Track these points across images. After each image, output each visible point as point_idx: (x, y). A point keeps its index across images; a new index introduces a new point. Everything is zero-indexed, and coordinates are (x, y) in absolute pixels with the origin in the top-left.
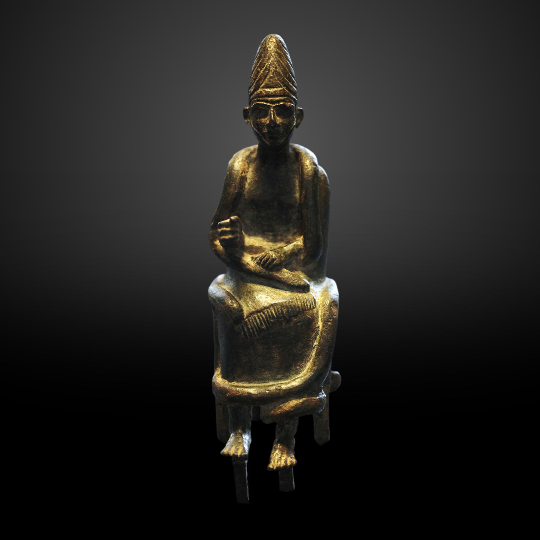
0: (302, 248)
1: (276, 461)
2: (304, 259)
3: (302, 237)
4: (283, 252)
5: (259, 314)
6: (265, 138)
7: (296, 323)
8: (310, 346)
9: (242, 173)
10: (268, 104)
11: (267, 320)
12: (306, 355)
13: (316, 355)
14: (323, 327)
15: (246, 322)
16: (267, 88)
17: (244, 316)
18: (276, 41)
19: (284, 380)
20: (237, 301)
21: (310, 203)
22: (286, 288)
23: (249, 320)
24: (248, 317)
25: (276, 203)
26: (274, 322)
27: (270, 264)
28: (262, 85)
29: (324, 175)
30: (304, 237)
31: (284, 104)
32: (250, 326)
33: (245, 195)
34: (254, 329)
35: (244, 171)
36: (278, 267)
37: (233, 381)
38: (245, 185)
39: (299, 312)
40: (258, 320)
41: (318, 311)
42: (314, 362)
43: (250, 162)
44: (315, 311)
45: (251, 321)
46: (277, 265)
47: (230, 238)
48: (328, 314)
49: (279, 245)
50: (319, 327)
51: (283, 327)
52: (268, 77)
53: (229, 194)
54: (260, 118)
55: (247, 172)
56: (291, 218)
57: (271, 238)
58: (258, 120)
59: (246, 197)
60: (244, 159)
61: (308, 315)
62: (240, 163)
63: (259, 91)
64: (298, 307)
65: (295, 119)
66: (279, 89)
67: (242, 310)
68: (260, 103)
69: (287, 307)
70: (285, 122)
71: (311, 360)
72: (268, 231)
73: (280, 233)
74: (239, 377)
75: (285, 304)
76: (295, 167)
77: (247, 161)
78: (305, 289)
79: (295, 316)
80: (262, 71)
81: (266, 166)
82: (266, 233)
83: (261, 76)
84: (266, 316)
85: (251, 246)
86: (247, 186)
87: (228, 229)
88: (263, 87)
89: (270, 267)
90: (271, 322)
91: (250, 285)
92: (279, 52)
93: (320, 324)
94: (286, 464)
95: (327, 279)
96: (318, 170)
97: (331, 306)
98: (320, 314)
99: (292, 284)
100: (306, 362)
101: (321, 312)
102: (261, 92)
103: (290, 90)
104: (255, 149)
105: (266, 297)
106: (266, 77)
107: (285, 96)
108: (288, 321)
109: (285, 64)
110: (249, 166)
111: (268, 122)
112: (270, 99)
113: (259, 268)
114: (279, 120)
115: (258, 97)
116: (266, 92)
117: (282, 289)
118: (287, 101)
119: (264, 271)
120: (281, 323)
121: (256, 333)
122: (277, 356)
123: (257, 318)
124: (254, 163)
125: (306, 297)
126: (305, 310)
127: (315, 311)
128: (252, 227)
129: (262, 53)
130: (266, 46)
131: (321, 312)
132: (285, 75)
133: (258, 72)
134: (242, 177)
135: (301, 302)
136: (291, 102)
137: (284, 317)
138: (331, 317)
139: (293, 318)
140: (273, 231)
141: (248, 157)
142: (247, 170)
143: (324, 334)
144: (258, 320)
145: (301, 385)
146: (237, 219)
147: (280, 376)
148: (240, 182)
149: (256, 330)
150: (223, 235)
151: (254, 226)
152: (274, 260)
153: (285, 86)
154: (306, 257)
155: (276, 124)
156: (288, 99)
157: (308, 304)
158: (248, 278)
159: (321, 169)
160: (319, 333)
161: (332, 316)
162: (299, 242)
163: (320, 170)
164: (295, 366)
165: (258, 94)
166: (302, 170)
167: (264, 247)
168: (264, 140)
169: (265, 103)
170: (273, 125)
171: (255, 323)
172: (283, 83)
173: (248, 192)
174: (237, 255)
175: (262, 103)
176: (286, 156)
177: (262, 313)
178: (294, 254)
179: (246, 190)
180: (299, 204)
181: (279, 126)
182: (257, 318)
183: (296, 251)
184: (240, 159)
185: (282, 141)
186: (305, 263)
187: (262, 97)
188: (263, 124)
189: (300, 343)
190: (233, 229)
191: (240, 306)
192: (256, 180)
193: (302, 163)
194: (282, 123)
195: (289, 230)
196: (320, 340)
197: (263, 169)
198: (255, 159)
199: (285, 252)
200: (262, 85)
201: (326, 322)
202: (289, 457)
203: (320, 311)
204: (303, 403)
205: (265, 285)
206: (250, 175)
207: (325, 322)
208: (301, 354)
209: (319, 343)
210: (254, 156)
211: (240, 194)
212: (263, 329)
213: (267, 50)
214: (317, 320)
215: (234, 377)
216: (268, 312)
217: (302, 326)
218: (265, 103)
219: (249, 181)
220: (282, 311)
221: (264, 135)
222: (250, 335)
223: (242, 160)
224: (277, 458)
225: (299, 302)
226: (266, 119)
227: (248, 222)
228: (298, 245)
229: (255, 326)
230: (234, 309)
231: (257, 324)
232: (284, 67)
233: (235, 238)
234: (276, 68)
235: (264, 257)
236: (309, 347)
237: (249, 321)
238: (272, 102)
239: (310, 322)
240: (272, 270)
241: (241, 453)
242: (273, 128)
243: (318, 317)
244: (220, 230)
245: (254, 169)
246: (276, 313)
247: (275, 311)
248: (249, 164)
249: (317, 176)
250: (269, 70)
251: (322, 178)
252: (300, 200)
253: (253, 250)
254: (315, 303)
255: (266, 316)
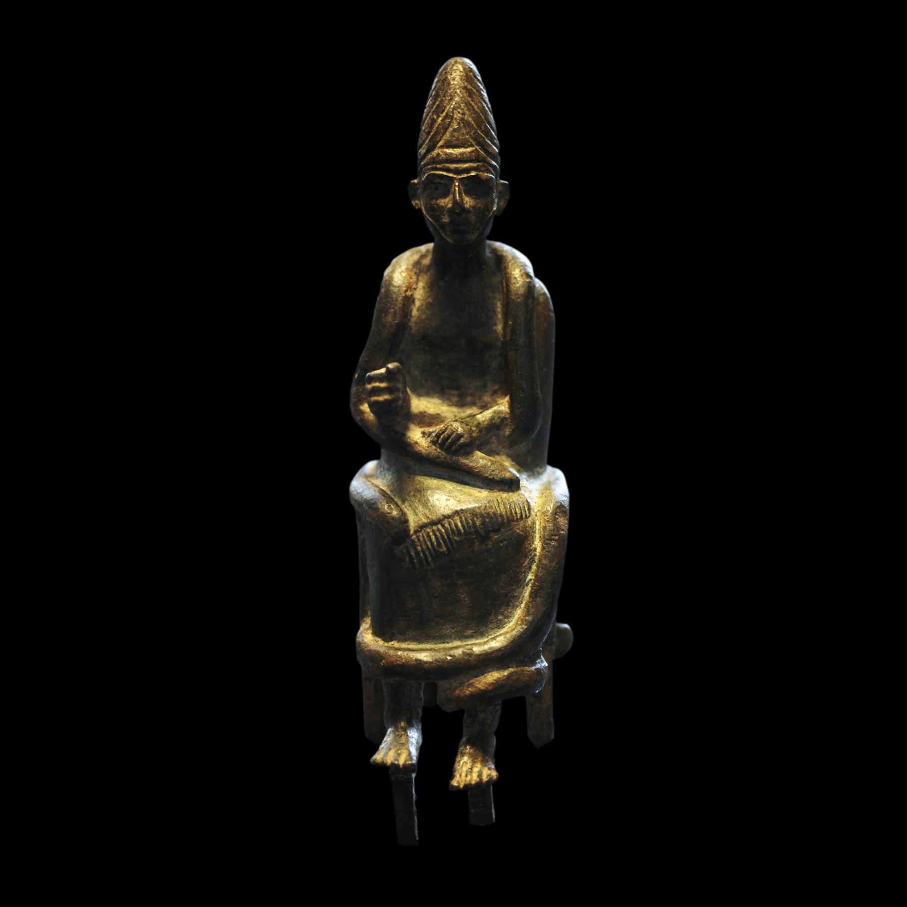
0: (508, 416)
1: (464, 774)
2: (510, 436)
3: (507, 398)
4: (476, 422)
5: (435, 528)
6: (445, 231)
7: (497, 542)
8: (520, 580)
9: (406, 291)
10: (451, 175)
11: (449, 538)
12: (514, 597)
13: (530, 596)
14: (543, 548)
15: (413, 542)
16: (448, 147)
17: (409, 531)
18: (464, 69)
19: (477, 639)
20: (398, 506)
21: (522, 340)
22: (480, 484)
23: (418, 537)
24: (416, 532)
25: (464, 340)
26: (461, 541)
27: (453, 443)
28: (441, 143)
29: (544, 294)
30: (511, 399)
31: (477, 175)
32: (419, 548)
33: (411, 328)
34: (427, 553)
35: (409, 287)
36: (467, 448)
37: (391, 640)
38: (411, 310)
39: (502, 524)
40: (433, 537)
41: (534, 523)
42: (527, 607)
43: (421, 271)
44: (530, 523)
45: (421, 539)
46: (464, 445)
47: (386, 400)
48: (552, 528)
49: (469, 411)
50: (535, 550)
51: (476, 549)
52: (450, 129)
53: (384, 326)
54: (437, 199)
55: (415, 289)
56: (489, 367)
57: (455, 399)
58: (433, 202)
59: (413, 331)
60: (411, 267)
61: (518, 529)
62: (404, 274)
63: (434, 153)
64: (501, 515)
65: (496, 200)
66: (469, 150)
67: (407, 521)
68: (438, 172)
69: (481, 515)
70: (478, 205)
71: (523, 606)
72: (450, 388)
73: (470, 391)
74: (401, 634)
75: (479, 511)
76: (496, 280)
77: (415, 270)
78: (512, 485)
79: (496, 531)
80: (440, 119)
81: (446, 279)
82: (447, 391)
83: (438, 128)
84: (446, 530)
85: (421, 413)
86: (415, 312)
87: (383, 385)
88: (442, 147)
89: (454, 448)
90: (456, 541)
91: (419, 478)
92: (469, 87)
93: (537, 544)
94: (481, 780)
95: (550, 469)
96: (534, 286)
97: (556, 514)
98: (538, 527)
99: (491, 477)
100: (515, 607)
101: (539, 524)
102: (438, 154)
103: (486, 151)
104: (428, 251)
105: (446, 499)
106: (447, 129)
107: (479, 161)
108: (484, 539)
109: (478, 108)
110: (418, 279)
111: (450, 205)
112: (453, 166)
113: (434, 450)
114: (468, 202)
115: (433, 163)
116: (446, 154)
117: (474, 486)
118: (483, 169)
119: (443, 454)
120: (472, 543)
121: (430, 559)
122: (465, 598)
123: (431, 534)
124: (426, 273)
125: (515, 499)
126: (513, 521)
127: (530, 523)
128: (423, 382)
129: (440, 89)
130: (446, 78)
131: (539, 524)
132: (479, 127)
133: (434, 121)
134: (406, 297)
135: (505, 508)
136: (488, 171)
137: (477, 532)
138: (556, 533)
139: (492, 534)
140: (458, 388)
141: (417, 264)
142: (414, 286)
143: (544, 562)
144: (433, 537)
145: (505, 647)
146: (398, 367)
147: (469, 632)
148: (404, 305)
149: (431, 554)
150: (375, 395)
151: (426, 380)
152: (460, 436)
153: (478, 144)
154: (513, 431)
155: (463, 209)
156: (483, 166)
157: (518, 511)
158: (416, 468)
159: (539, 284)
160: (536, 559)
161: (558, 531)
162: (503, 406)
163: (537, 285)
164: (496, 614)
165: (433, 158)
166: (507, 286)
167: (443, 415)
168: (443, 235)
169: (445, 173)
170: (458, 209)
171: (429, 543)
172: (475, 139)
173: (416, 323)
174: (398, 429)
175: (441, 173)
176: (480, 262)
177: (440, 526)
178: (494, 426)
179: (413, 320)
180: (503, 343)
181: (468, 211)
182: (431, 534)
183: (497, 421)
184: (403, 268)
185: (473, 237)
186: (512, 442)
187: (440, 162)
188: (441, 209)
189: (504, 576)
190: (391, 385)
191: (403, 514)
192: (429, 303)
193: (508, 273)
194: (473, 207)
195: (485, 386)
196: (537, 571)
197: (442, 284)
198: (429, 267)
199: (479, 424)
200: (441, 143)
201: (548, 542)
202: (486, 768)
203: (538, 523)
204: (508, 677)
205: (445, 479)
206: (419, 294)
207: (546, 541)
208: (506, 595)
209: (536, 576)
210: (427, 261)
211: (403, 327)
212: (442, 553)
213: (449, 83)
214: (533, 538)
215: (393, 634)
216: (450, 524)
217: (506, 547)
218: (445, 173)
219: (418, 304)
220: (474, 523)
221: (443, 226)
222: (421, 563)
223: (407, 269)
224: (464, 769)
225: (502, 506)
226: (447, 200)
227: (416, 373)
228: (500, 412)
229: (428, 547)
230: (393, 518)
231: (432, 544)
232: (476, 112)
233: (395, 400)
234: (464, 114)
235: (444, 432)
236: (519, 582)
237: (419, 540)
238: (458, 172)
239: (521, 541)
240: (456, 453)
241: (406, 761)
242: (459, 215)
243: (534, 532)
244: (369, 386)
245: (426, 284)
246: (463, 526)
247: (461, 522)
248: (418, 275)
249: (533, 296)
250: (452, 118)
251: (541, 299)
252: (504, 335)
253: (424, 419)
254: (529, 509)
255: (446, 530)
